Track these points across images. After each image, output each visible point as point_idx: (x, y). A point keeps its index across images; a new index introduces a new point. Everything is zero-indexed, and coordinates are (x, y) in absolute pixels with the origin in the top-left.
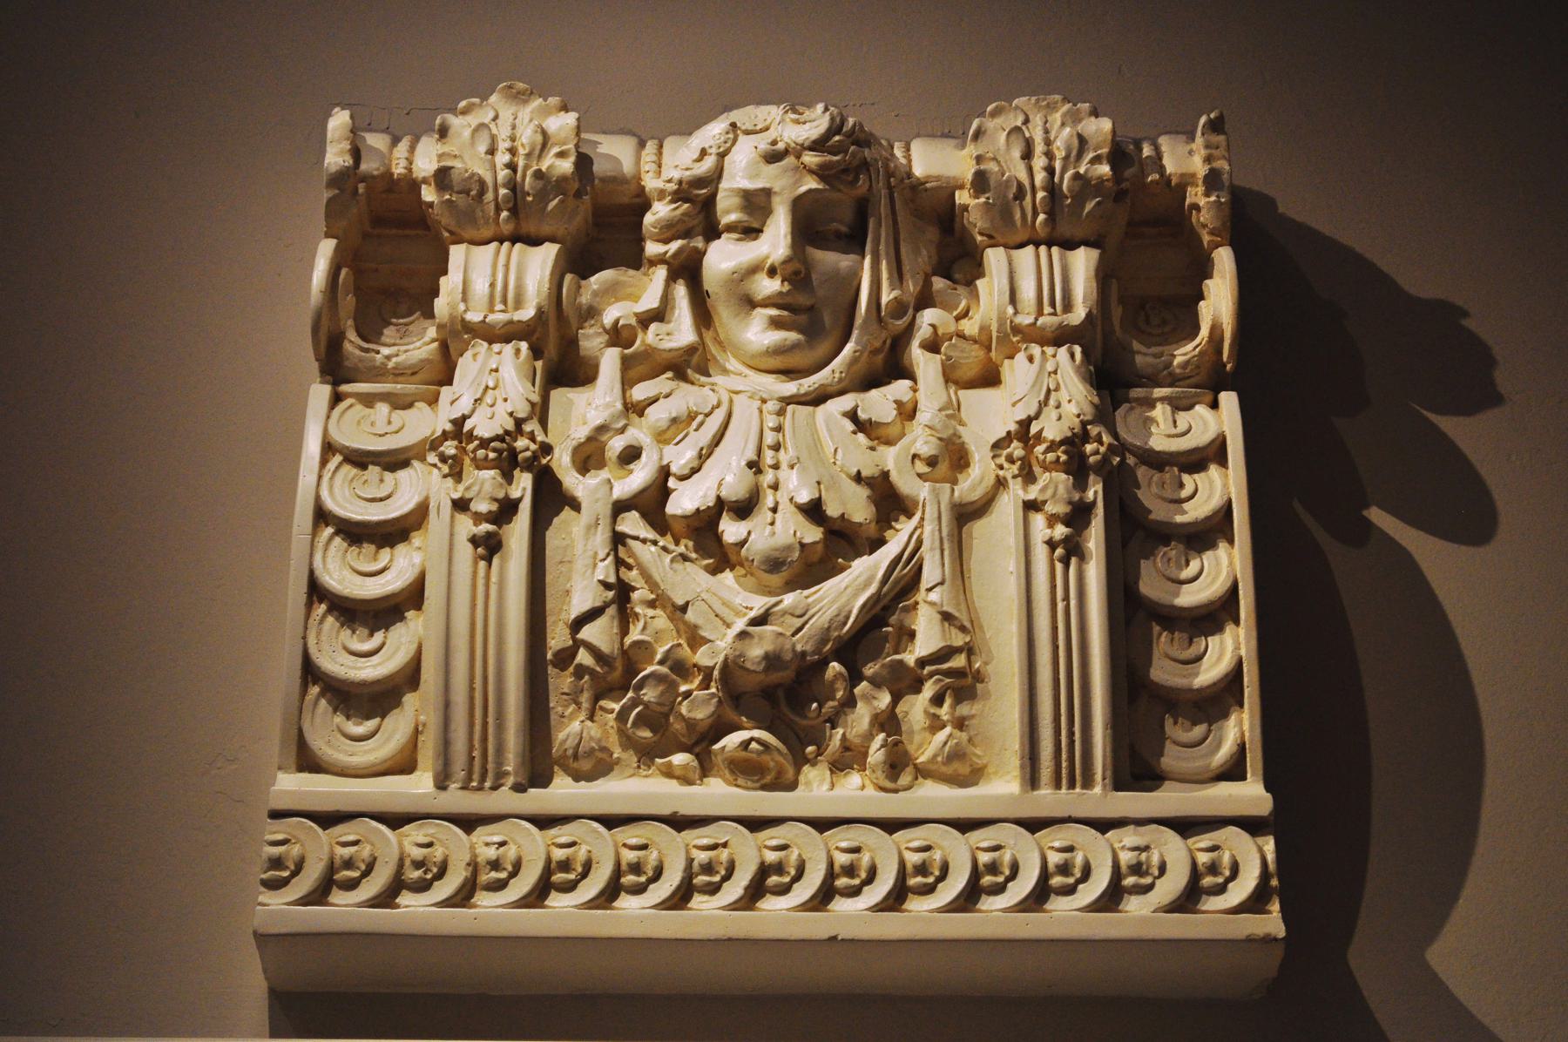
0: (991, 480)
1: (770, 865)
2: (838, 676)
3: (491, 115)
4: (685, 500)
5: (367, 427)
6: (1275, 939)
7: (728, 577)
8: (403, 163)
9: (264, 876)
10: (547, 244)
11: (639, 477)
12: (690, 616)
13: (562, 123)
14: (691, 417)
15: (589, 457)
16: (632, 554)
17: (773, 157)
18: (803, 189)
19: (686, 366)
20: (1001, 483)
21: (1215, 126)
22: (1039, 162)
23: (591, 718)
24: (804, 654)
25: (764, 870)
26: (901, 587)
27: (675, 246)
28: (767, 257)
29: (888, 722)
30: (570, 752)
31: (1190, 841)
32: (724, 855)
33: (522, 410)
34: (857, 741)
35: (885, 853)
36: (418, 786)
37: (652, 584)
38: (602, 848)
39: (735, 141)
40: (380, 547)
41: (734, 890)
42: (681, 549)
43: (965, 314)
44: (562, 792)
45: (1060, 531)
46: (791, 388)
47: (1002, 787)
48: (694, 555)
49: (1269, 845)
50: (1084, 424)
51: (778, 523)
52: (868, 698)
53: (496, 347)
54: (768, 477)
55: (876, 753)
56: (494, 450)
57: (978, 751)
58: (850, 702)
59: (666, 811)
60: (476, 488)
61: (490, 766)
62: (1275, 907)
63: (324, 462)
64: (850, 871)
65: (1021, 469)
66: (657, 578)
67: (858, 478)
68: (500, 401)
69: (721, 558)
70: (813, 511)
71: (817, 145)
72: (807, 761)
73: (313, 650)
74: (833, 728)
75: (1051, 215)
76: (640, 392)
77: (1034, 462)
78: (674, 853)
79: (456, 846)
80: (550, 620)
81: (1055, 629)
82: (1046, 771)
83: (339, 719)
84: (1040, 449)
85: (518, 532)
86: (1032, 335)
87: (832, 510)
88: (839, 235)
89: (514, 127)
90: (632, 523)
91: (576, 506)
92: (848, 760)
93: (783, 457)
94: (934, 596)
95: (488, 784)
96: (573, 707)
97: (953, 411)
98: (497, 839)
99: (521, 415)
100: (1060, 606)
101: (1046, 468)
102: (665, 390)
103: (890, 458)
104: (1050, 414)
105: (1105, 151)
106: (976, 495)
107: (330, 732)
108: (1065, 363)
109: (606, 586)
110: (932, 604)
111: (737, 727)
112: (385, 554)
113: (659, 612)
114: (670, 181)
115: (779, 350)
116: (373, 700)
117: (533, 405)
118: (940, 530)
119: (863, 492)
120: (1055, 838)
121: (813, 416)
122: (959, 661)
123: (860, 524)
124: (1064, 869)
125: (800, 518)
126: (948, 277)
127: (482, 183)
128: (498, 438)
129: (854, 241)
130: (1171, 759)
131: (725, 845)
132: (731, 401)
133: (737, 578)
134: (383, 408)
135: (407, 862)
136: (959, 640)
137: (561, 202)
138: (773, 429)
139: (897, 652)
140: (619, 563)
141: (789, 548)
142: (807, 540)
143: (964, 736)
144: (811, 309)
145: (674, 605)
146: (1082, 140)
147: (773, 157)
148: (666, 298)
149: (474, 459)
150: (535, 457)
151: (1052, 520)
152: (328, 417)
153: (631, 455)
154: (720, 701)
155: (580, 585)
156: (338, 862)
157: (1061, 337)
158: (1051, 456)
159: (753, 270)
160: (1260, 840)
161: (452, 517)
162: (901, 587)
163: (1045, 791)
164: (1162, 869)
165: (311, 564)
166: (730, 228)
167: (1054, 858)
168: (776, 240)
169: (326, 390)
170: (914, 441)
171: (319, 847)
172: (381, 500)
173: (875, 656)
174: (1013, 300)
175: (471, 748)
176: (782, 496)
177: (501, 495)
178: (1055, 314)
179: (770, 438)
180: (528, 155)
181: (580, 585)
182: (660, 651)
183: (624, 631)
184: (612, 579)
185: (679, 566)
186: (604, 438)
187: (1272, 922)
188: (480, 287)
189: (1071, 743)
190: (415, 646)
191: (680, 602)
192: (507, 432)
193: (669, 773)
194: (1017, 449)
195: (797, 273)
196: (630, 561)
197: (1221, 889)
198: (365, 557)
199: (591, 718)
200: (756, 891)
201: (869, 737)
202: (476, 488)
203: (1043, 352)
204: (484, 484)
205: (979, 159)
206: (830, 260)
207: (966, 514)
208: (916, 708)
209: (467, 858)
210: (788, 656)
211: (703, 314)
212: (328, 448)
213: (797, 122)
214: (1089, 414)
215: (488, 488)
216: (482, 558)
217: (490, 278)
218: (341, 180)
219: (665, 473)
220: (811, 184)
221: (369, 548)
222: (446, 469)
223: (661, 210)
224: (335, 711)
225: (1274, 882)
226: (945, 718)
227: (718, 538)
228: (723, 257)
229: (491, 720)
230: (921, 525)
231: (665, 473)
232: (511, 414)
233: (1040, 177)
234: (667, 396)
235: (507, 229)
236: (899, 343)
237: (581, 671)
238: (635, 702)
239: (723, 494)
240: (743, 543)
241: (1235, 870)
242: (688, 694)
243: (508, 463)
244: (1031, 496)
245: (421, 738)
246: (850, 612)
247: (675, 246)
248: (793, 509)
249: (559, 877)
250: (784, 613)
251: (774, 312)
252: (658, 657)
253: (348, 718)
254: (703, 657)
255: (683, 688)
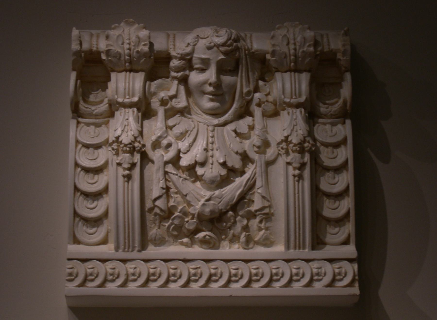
0: (276, 154)
1: (213, 274)
2: (232, 216)
3: (122, 30)
4: (185, 161)
5: (89, 134)
6: (357, 295)
7: (198, 184)
8: (95, 46)
9: (67, 278)
10: (140, 73)
11: (171, 153)
12: (188, 198)
13: (144, 33)
14: (187, 132)
15: (156, 145)
16: (170, 178)
17: (209, 48)
18: (220, 58)
19: (184, 112)
20: (279, 154)
21: (346, 34)
22: (292, 47)
23: (159, 228)
24: (221, 210)
25: (211, 276)
26: (250, 187)
27: (180, 74)
28: (209, 80)
29: (246, 228)
30: (153, 239)
31: (333, 265)
32: (199, 271)
33: (137, 134)
34: (237, 234)
35: (246, 270)
36: (108, 250)
37: (176, 188)
38: (164, 269)
39: (198, 41)
40: (95, 174)
41: (202, 281)
42: (184, 176)
43: (268, 94)
44: (152, 251)
45: (297, 172)
46: (216, 121)
47: (279, 248)
48: (188, 178)
49: (356, 266)
50: (304, 137)
51: (213, 168)
52: (241, 221)
53: (127, 110)
54: (210, 153)
55: (243, 238)
56: (129, 148)
57: (272, 237)
58: (235, 222)
59: (182, 258)
60: (124, 160)
61: (131, 245)
62: (357, 285)
63: (76, 146)
64: (235, 275)
65: (285, 152)
66: (178, 186)
67: (237, 153)
68: (129, 130)
69: (197, 178)
70: (224, 165)
71: (224, 44)
72: (222, 240)
73: (76, 208)
74: (230, 230)
75: (295, 62)
76: (171, 122)
77: (289, 149)
78: (185, 270)
79: (121, 268)
80: (146, 198)
81: (295, 202)
82: (292, 245)
83: (85, 228)
84: (291, 145)
85: (136, 172)
86: (290, 105)
87: (229, 164)
88: (230, 71)
89: (129, 34)
90: (170, 168)
91: (153, 162)
92: (234, 239)
93: (215, 146)
94: (259, 191)
95: (130, 250)
96: (153, 225)
97: (265, 129)
98: (134, 266)
99: (136, 136)
100: (297, 195)
101: (293, 152)
102: (178, 122)
103: (247, 144)
104: (294, 134)
105: (312, 43)
106: (272, 158)
107: (82, 231)
108: (299, 115)
109: (163, 188)
110: (259, 193)
111: (202, 231)
112: (96, 177)
113: (178, 195)
114: (178, 54)
115: (212, 109)
116: (96, 222)
117: (139, 131)
118: (261, 170)
119: (238, 157)
120: (294, 265)
121: (223, 131)
122: (267, 211)
123: (238, 168)
124: (297, 274)
125: (220, 167)
126: (264, 80)
127: (120, 54)
128: (130, 144)
129: (234, 71)
130: (329, 238)
131: (199, 268)
132: (198, 125)
133: (201, 184)
134: (92, 127)
135: (108, 274)
136: (267, 204)
137: (145, 60)
138: (211, 137)
139: (248, 207)
140: (166, 180)
141: (216, 177)
142: (222, 174)
143: (268, 232)
144: (222, 95)
145: (183, 195)
146: (304, 38)
147: (209, 48)
148: (177, 91)
149: (122, 150)
150: (141, 149)
151: (295, 168)
152: (76, 131)
153: (169, 145)
154: (197, 224)
155: (155, 190)
156: (88, 274)
157: (298, 106)
158: (294, 148)
159: (205, 83)
160: (353, 265)
161: (117, 168)
162: (250, 187)
163: (291, 251)
164: (325, 274)
165: (74, 181)
166: (197, 69)
167: (294, 271)
168: (211, 75)
169: (75, 121)
170: (254, 140)
171: (82, 269)
172: (94, 160)
173: (242, 209)
174: (284, 93)
175: (125, 239)
176: (215, 160)
177: (131, 162)
178: (296, 98)
179: (210, 140)
180: (134, 46)
181: (155, 190)
182: (180, 208)
183: (168, 201)
184: (165, 187)
185: (184, 182)
186: (160, 140)
187: (356, 290)
188: (121, 85)
189: (299, 236)
190: (106, 206)
191: (185, 194)
192: (132, 141)
193: (182, 244)
194: (284, 145)
195: (218, 85)
196: (169, 179)
197: (341, 280)
198: (89, 178)
199: (159, 228)
200: (209, 280)
201: (241, 233)
202: (124, 160)
203: (293, 111)
204: (125, 157)
205: (274, 45)
206: (227, 79)
207: (269, 163)
208: (254, 223)
209: (125, 273)
210: (217, 211)
211: (189, 93)
212: (77, 142)
213: (217, 36)
214: (306, 134)
215: (127, 160)
216: (127, 182)
217: (125, 85)
218: (77, 53)
219: (179, 151)
220: (222, 57)
221: (91, 175)
222: (114, 152)
223: (175, 63)
224: (84, 225)
225: (357, 278)
226: (263, 227)
227: (196, 173)
228: (195, 78)
229: (131, 231)
230: (256, 168)
231: (179, 151)
232: (133, 135)
233: (292, 52)
234: (178, 124)
235: (128, 68)
236: (249, 103)
237: (156, 214)
238: (172, 224)
239: (197, 160)
240: (203, 175)
241: (346, 274)
242: (187, 222)
243: (132, 151)
244: (288, 161)
245: (109, 234)
246: (235, 197)
247: (180, 74)
248: (217, 164)
249: (152, 278)
250: (216, 197)
251: (211, 97)
252: (179, 210)
253: (87, 227)
254: (191, 210)
255: (186, 220)
